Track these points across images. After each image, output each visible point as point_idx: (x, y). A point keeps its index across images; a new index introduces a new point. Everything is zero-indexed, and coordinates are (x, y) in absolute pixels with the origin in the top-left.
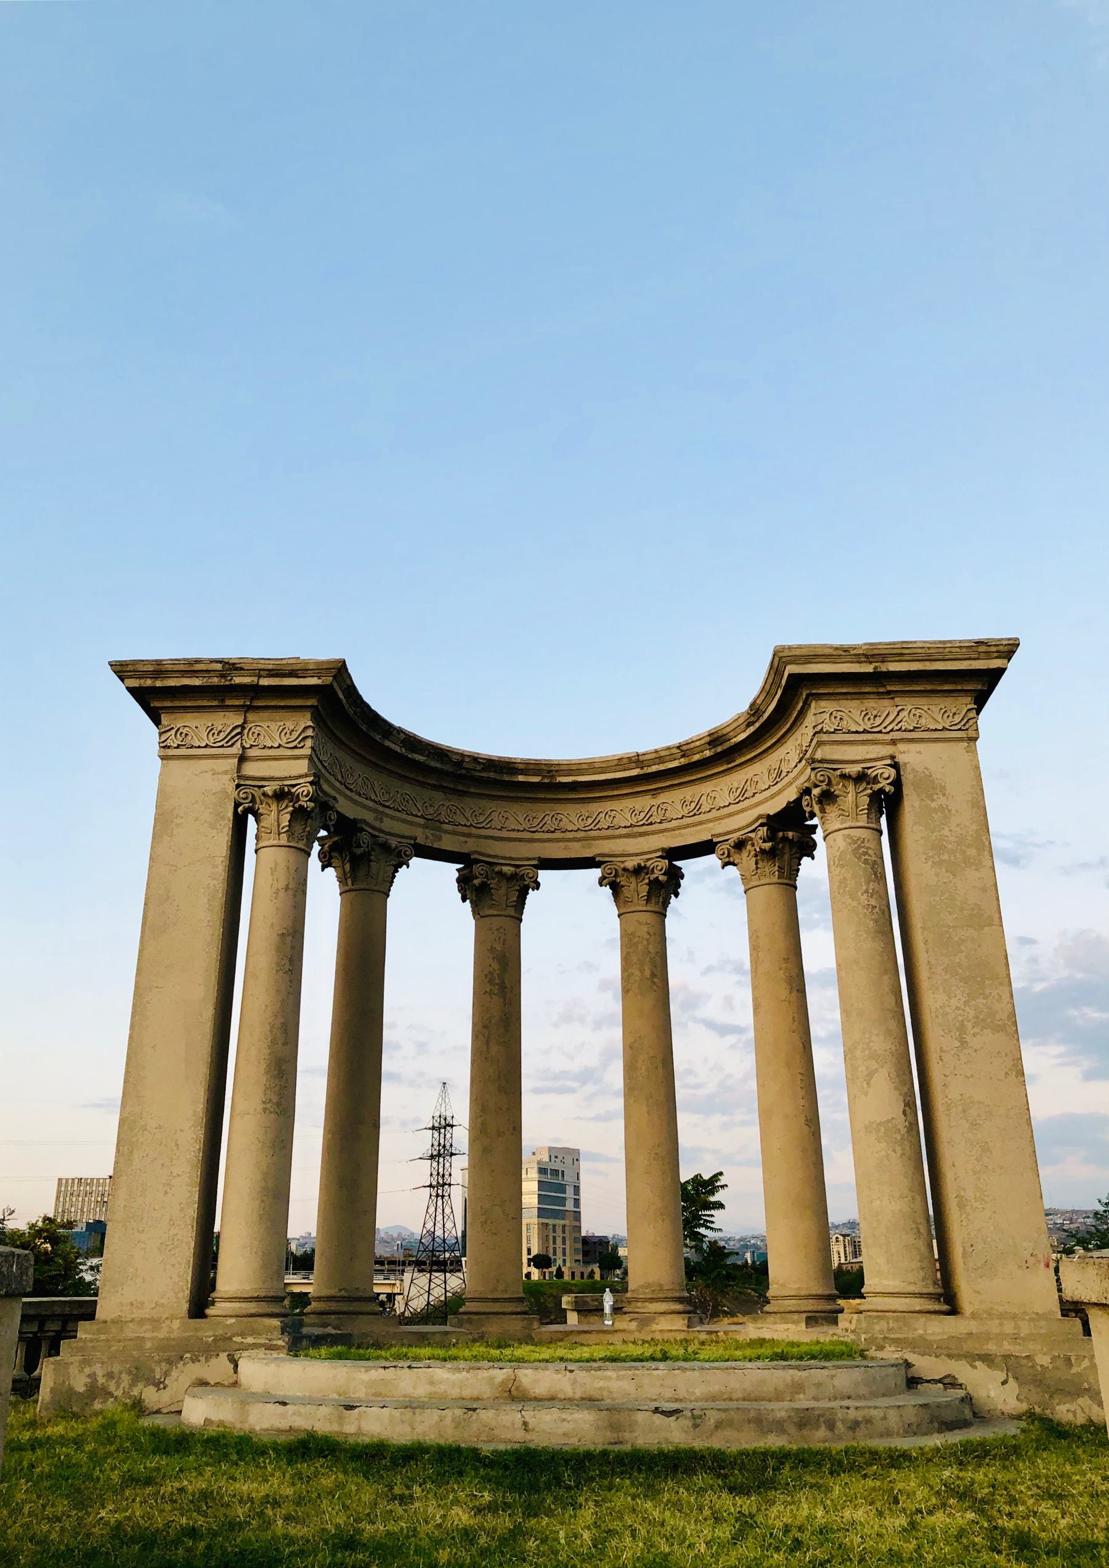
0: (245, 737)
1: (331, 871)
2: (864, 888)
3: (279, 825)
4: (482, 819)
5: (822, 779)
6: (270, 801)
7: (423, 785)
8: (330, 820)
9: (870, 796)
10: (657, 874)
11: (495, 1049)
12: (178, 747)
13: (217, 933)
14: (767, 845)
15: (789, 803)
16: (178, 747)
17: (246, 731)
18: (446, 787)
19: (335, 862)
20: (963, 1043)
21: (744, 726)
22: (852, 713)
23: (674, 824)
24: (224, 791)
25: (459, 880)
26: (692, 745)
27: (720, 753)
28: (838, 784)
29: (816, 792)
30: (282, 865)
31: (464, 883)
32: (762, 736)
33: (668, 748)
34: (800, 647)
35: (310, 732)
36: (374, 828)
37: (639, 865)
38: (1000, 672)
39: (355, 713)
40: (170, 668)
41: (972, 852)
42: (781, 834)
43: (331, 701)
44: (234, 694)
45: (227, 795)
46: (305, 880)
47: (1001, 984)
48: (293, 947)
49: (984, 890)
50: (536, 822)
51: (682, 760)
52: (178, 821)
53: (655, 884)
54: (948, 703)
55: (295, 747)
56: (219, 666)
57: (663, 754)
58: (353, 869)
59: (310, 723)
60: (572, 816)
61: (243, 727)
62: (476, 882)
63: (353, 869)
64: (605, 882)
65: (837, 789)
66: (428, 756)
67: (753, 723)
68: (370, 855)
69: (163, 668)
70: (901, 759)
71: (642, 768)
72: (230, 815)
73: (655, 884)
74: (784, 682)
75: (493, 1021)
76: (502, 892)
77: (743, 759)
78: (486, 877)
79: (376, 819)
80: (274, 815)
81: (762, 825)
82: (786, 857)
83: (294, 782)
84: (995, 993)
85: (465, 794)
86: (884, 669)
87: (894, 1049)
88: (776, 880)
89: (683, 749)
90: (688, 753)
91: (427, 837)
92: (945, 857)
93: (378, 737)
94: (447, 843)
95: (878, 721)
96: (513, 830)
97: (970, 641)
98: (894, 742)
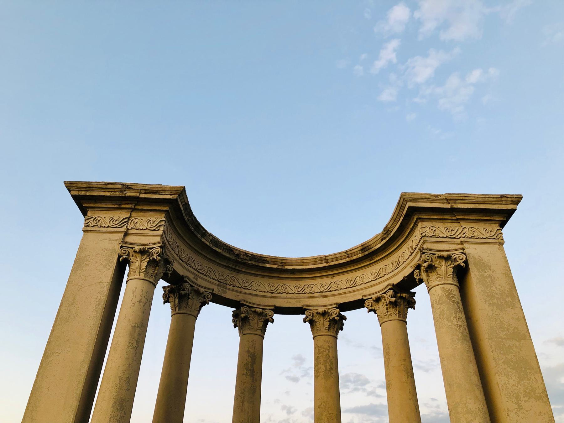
0: (129, 224)
1: (168, 305)
2: (454, 315)
3: (140, 269)
4: (247, 284)
5: (428, 258)
6: (137, 255)
7: (220, 265)
8: (169, 271)
9: (453, 268)
10: (334, 316)
11: (246, 404)
12: (93, 226)
13: (97, 324)
14: (393, 300)
15: (405, 277)
16: (93, 226)
17: (130, 221)
18: (231, 268)
19: (171, 299)
20: (520, 407)
21: (380, 240)
22: (441, 229)
23: (343, 291)
24: (114, 249)
25: (233, 316)
26: (353, 251)
27: (367, 255)
28: (436, 261)
29: (426, 264)
30: (138, 292)
31: (236, 316)
32: (384, 249)
33: (341, 253)
34: (414, 194)
35: (163, 223)
36: (192, 282)
37: (325, 311)
38: (513, 211)
39: (188, 220)
40: (95, 186)
41: (509, 299)
42: (399, 295)
43: (175, 208)
44: (126, 202)
45: (115, 251)
46: (151, 299)
47: (536, 372)
48: (139, 335)
49: (518, 319)
50: (274, 288)
51: (347, 259)
52: (87, 263)
53: (333, 321)
54: (487, 226)
55: (155, 230)
56: (120, 187)
57: (337, 256)
58: (179, 302)
59: (164, 219)
60: (291, 286)
61: (129, 219)
62: (242, 316)
63: (179, 302)
64: (307, 320)
65: (436, 264)
66: (223, 250)
67: (385, 238)
68: (189, 295)
69: (91, 186)
70: (466, 251)
71: (327, 263)
72: (115, 261)
73: (333, 321)
74: (404, 213)
75: (246, 390)
76: (256, 322)
77: (378, 259)
78: (248, 313)
79: (194, 278)
80: (138, 262)
81: (390, 289)
82: (402, 306)
83: (151, 247)
84: (533, 377)
85: (239, 272)
86: (455, 207)
87: (480, 408)
88: (397, 318)
89: (348, 253)
90: (350, 255)
91: (219, 291)
92: (495, 301)
93: (199, 236)
94: (229, 295)
95: (453, 233)
96: (262, 291)
97: (497, 195)
98: (462, 243)
